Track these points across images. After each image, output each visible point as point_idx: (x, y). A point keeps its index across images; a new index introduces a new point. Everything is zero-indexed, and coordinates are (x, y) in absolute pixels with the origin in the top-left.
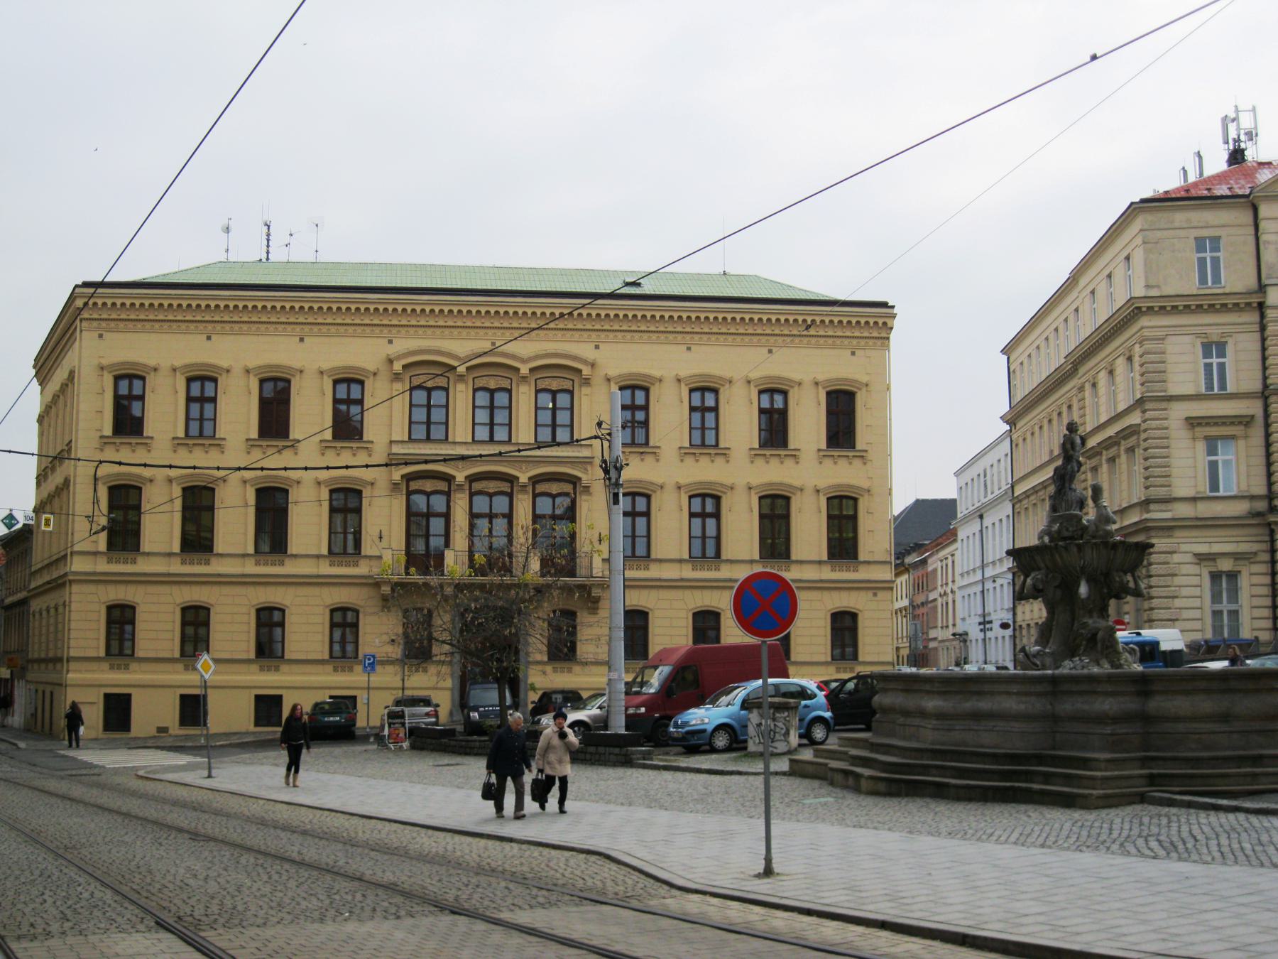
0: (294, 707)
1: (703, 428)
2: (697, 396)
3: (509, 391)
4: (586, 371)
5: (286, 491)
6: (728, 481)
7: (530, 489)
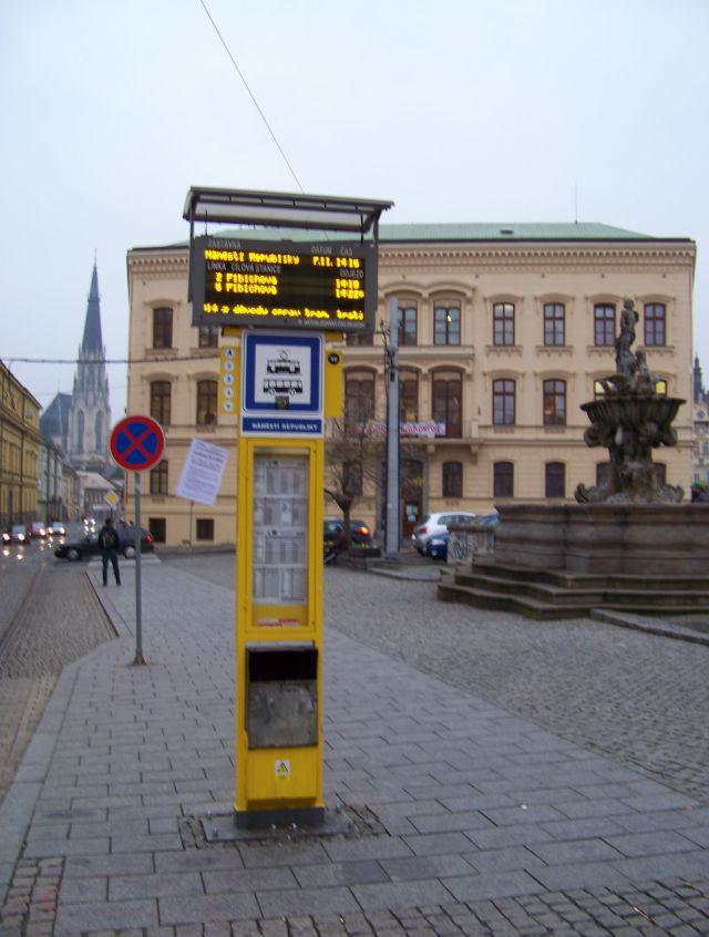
0: (439, 523)
1: (654, 332)
2: (650, 309)
3: (416, 310)
4: (469, 294)
5: (169, 383)
6: (571, 370)
7: (430, 377)
